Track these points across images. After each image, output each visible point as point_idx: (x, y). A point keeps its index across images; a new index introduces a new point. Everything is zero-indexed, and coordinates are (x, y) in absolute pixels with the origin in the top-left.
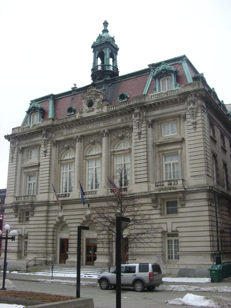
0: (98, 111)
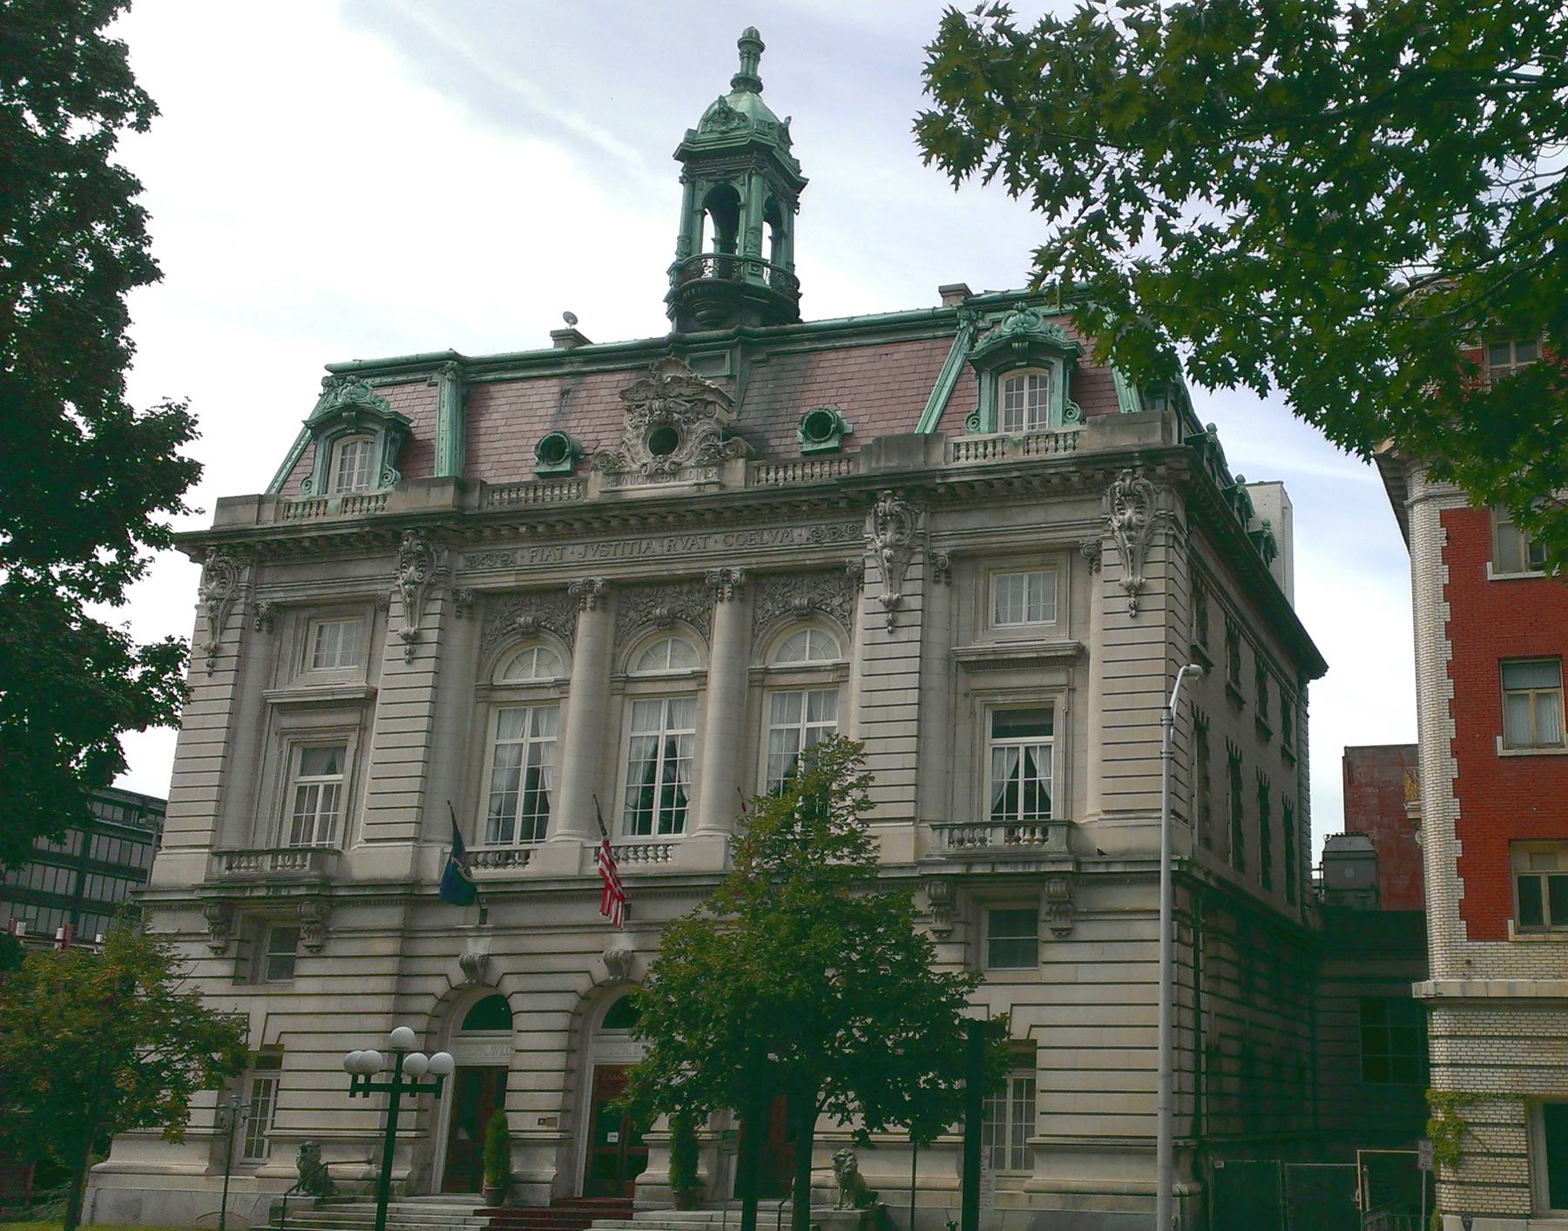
0: (703, 480)
